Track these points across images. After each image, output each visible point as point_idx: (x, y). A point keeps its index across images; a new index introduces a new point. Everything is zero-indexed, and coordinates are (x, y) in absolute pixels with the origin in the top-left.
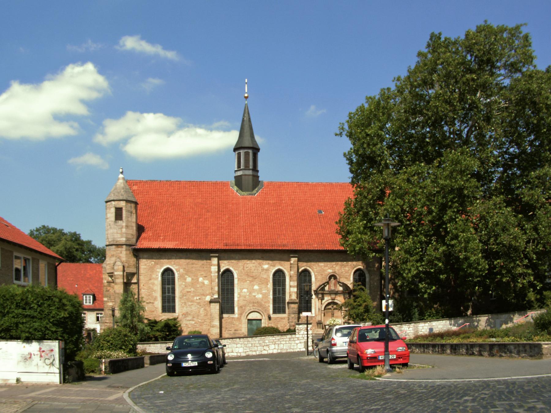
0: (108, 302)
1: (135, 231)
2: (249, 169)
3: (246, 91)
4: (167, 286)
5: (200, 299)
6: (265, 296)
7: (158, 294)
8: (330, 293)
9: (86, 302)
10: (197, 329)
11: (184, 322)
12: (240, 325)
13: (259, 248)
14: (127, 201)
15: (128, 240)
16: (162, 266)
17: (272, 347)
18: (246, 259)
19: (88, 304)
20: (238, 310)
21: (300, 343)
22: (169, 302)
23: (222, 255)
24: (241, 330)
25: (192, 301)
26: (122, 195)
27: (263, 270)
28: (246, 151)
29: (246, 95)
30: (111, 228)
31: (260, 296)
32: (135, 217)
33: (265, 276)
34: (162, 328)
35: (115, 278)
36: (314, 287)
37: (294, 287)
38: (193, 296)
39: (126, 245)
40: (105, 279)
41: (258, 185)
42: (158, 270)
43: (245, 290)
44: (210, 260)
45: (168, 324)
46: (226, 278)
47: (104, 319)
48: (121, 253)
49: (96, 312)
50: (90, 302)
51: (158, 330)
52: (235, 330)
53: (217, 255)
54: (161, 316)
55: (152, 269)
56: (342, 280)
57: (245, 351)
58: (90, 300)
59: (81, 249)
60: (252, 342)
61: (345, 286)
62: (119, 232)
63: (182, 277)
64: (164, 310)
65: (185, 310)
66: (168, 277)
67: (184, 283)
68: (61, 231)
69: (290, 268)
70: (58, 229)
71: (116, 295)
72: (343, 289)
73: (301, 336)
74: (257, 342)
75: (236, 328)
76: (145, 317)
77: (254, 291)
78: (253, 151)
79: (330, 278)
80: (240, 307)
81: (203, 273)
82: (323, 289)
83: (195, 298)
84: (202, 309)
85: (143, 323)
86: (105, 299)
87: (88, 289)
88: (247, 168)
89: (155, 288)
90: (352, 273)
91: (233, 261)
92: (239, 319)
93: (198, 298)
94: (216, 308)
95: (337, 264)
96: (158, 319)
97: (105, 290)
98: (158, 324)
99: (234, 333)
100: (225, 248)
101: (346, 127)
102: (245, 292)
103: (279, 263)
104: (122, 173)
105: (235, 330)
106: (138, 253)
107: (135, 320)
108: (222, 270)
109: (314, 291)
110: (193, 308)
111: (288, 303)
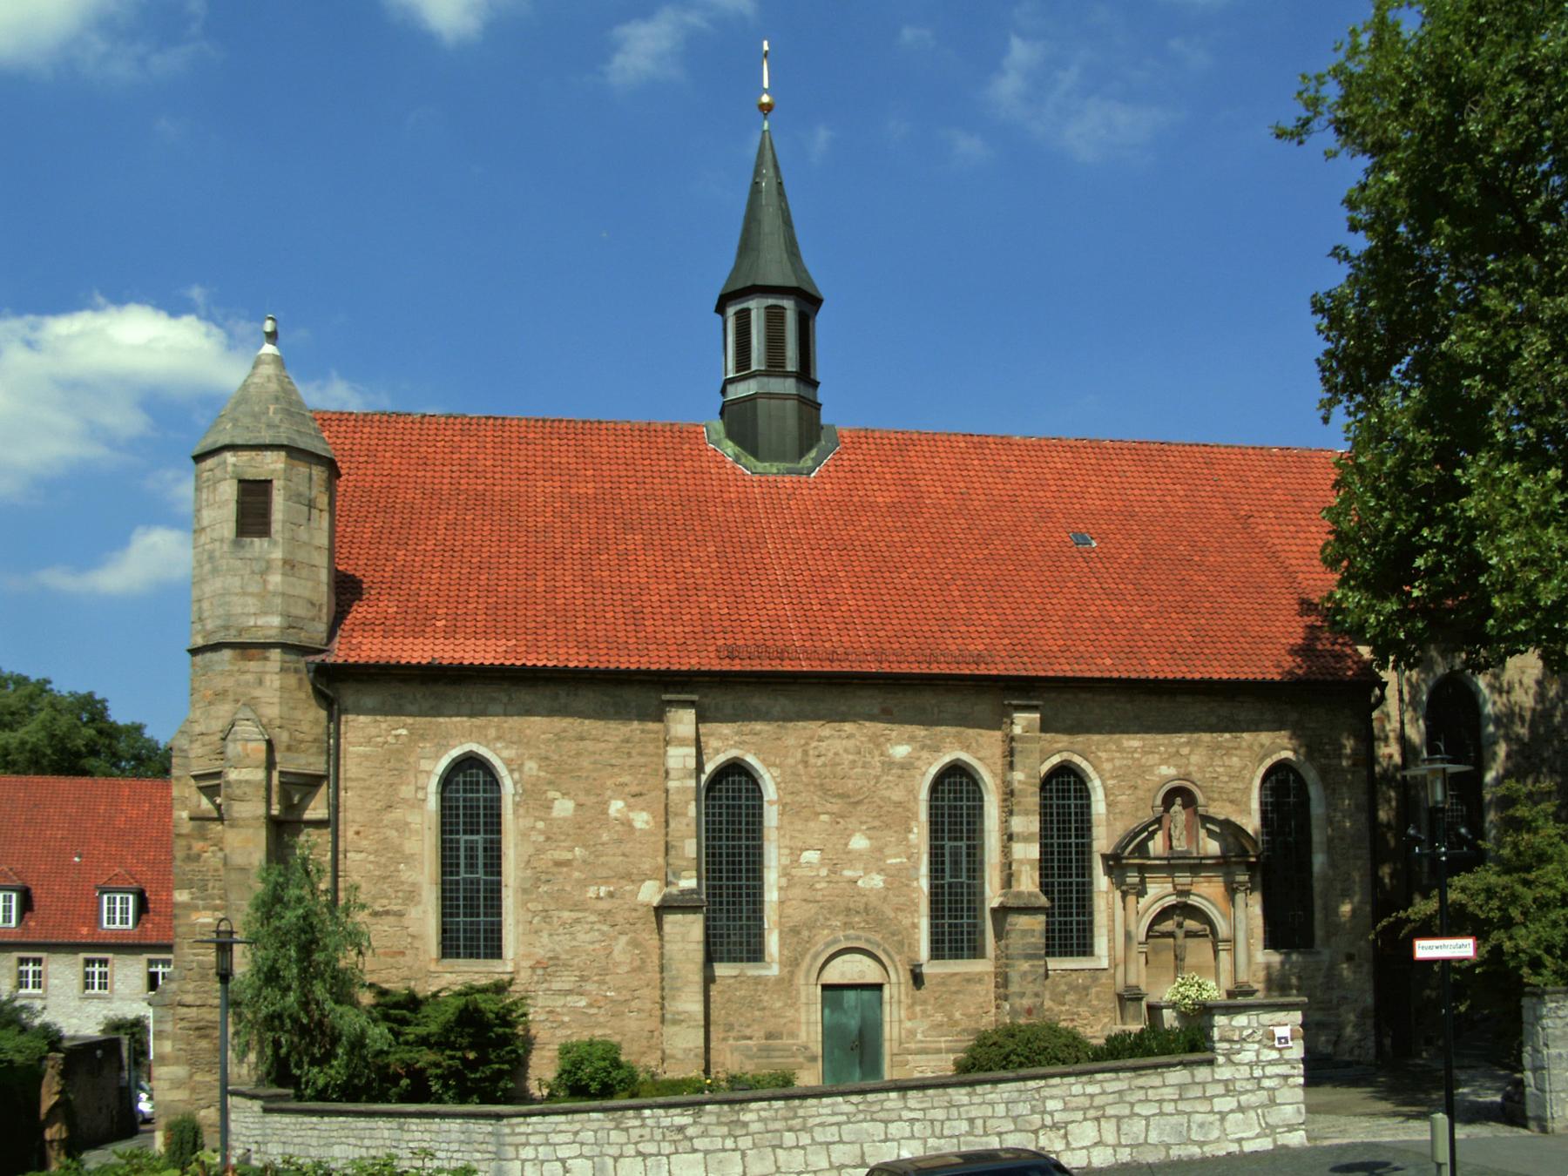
0: (196, 908)
1: (324, 588)
2: (787, 375)
3: (766, 85)
4: (463, 838)
5: (611, 895)
6: (899, 880)
7: (425, 874)
8: (1174, 865)
9: (112, 920)
10: (598, 1032)
11: (540, 1002)
12: (790, 1013)
13: (874, 668)
14: (294, 452)
15: (292, 624)
17: (1085, 1133)
18: (815, 717)
19: (118, 925)
20: (782, 945)
21: (1241, 1109)
22: (472, 910)
23: (713, 699)
24: (793, 1035)
26: (270, 426)
27: (889, 764)
28: (771, 301)
29: (765, 99)
30: (215, 571)
32: (325, 524)
33: (897, 795)
34: (447, 1029)
35: (230, 798)
36: (1102, 841)
37: (1026, 839)
38: (583, 884)
39: (285, 647)
40: (184, 802)
41: (818, 439)
42: (425, 765)
43: (811, 856)
44: (659, 718)
45: (477, 1010)
46: (731, 797)
47: (174, 986)
48: (261, 682)
49: (82, 956)
50: (124, 921)
51: (424, 1041)
52: (769, 1036)
53: (695, 697)
54: (438, 974)
55: (397, 762)
56: (1220, 811)
58: (124, 911)
59: (109, 746)
60: (974, 1112)
61: (1229, 831)
62: (253, 588)
63: (533, 797)
64: (450, 946)
65: (544, 946)
66: (470, 798)
67: (540, 825)
68: (42, 686)
69: (1008, 759)
70: (33, 679)
71: (234, 876)
72: (1225, 849)
73: (1244, 1071)
74: (1001, 1110)
75: (771, 1024)
76: (368, 979)
77: (851, 857)
78: (797, 304)
79: (1168, 800)
80: (791, 932)
81: (626, 779)
82: (1142, 849)
83: (591, 892)
84: (623, 939)
85: (355, 1004)
86: (181, 896)
87: (117, 870)
88: (775, 366)
89: (411, 846)
90: (1257, 782)
91: (758, 726)
92: (785, 984)
93: (603, 891)
94: (688, 932)
95: (1197, 743)
96: (424, 989)
97: (179, 854)
98: (426, 1010)
99: (766, 1051)
100: (726, 666)
101: (1332, 91)
102: (809, 864)
103: (957, 736)
104: (272, 337)
105: (769, 1036)
106: (336, 685)
107: (319, 990)
108: (709, 768)
109: (1105, 857)
110: (581, 937)
111: (1002, 912)
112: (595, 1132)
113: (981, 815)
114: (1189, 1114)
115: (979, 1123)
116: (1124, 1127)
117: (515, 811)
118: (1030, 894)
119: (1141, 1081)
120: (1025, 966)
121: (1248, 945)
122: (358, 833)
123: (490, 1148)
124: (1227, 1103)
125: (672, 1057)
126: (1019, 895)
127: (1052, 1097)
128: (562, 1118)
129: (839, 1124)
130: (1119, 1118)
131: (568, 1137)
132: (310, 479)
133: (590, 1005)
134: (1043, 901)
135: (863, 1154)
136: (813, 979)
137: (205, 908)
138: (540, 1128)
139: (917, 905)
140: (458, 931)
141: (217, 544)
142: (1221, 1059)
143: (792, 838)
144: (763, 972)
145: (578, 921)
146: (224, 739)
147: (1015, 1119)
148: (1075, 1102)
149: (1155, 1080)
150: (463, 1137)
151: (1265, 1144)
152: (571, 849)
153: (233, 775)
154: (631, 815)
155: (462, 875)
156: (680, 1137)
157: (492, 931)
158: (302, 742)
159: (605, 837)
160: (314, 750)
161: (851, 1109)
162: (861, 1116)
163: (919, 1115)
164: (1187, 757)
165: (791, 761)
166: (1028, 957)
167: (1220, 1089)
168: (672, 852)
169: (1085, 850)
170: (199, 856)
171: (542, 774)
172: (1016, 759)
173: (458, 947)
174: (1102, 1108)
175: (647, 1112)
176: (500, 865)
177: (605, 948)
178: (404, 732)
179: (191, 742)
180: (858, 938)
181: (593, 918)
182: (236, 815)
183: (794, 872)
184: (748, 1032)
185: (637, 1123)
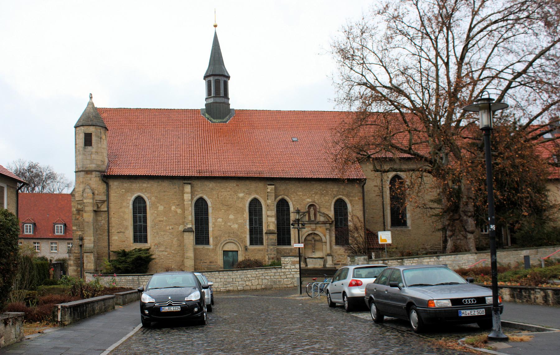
0: (78, 231)
4: (138, 215)
5: (172, 228)
6: (241, 226)
12: (215, 257)
16: (133, 194)
20: (213, 241)
24: (216, 262)
25: (164, 231)
27: (239, 198)
31: (236, 226)
33: (241, 205)
37: (271, 217)
42: (129, 198)
46: (201, 208)
50: (61, 232)
52: (211, 262)
64: (136, 240)
66: (139, 206)
67: (156, 212)
74: (238, 276)
80: (215, 238)
81: (176, 201)
83: (168, 228)
86: (74, 228)
90: (333, 203)
92: (214, 250)
93: (170, 227)
94: (190, 238)
102: (220, 222)
113: (262, 210)
119: (267, 272)
120: (272, 247)
121: (330, 244)
148: (253, 276)
153: (85, 201)
166: (272, 245)
167: (283, 274)
181: (168, 234)
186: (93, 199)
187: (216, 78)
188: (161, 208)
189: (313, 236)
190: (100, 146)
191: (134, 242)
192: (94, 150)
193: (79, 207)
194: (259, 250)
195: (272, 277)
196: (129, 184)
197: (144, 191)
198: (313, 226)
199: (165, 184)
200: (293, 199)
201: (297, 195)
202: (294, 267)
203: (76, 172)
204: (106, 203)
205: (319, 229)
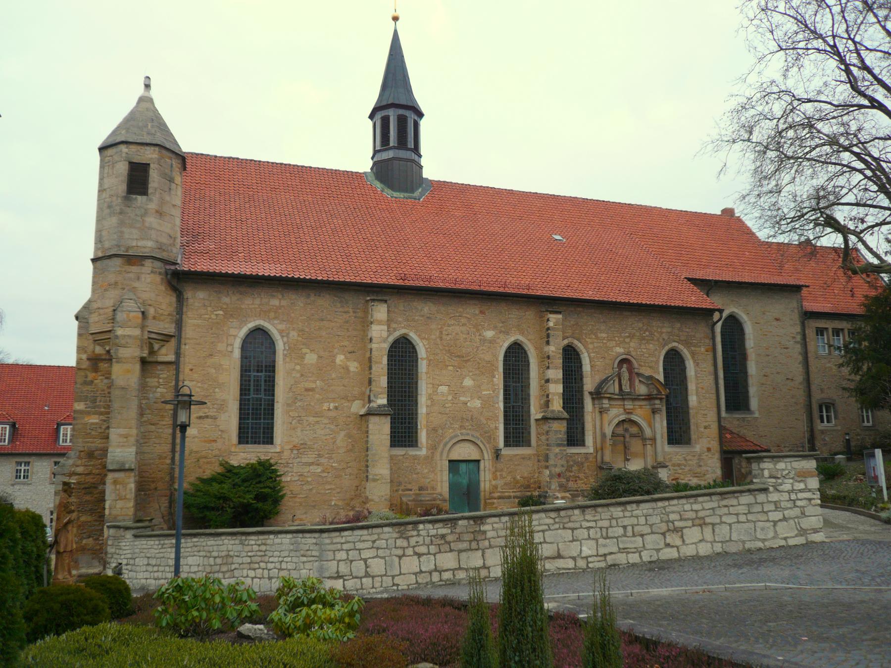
2: (391, 148)
5: (336, 408)
8: (623, 396)
12: (432, 476)
16: (243, 323)
17: (693, 534)
21: (785, 519)
24: (433, 488)
25: (316, 415)
27: (483, 340)
33: (488, 357)
36: (589, 385)
37: (556, 382)
42: (233, 332)
43: (443, 389)
46: (402, 355)
48: (138, 279)
52: (421, 489)
56: (647, 372)
57: (602, 551)
60: (626, 522)
61: (650, 380)
64: (244, 437)
67: (298, 367)
73: (786, 496)
74: (642, 520)
81: (346, 343)
90: (662, 358)
92: (429, 459)
93: (332, 406)
94: (380, 429)
100: (401, 283)
102: (443, 394)
105: (421, 489)
109: (591, 393)
112: (387, 540)
114: (754, 522)
115: (629, 529)
116: (717, 530)
117: (284, 359)
118: (559, 411)
119: (724, 502)
122: (191, 370)
123: (314, 553)
124: (776, 516)
125: (372, 500)
126: (553, 411)
127: (673, 512)
128: (365, 532)
129: (543, 531)
130: (713, 525)
131: (369, 544)
132: (172, 166)
133: (323, 471)
134: (566, 415)
135: (559, 550)
136: (444, 457)
137: (94, 414)
138: (350, 539)
139: (498, 417)
140: (248, 428)
141: (115, 198)
142: (771, 489)
143: (434, 378)
144: (418, 453)
145: (317, 422)
146: (114, 310)
147: (651, 526)
149: (734, 502)
150: (292, 547)
151: (801, 540)
152: (315, 382)
154: (348, 363)
155: (252, 396)
156: (443, 542)
157: (268, 428)
158: (162, 315)
159: (334, 376)
160: (168, 320)
161: (551, 521)
162: (557, 526)
163: (592, 524)
164: (629, 343)
165: (433, 337)
166: (559, 445)
167: (772, 507)
168: (373, 384)
169: (580, 390)
170: (92, 382)
171: (300, 339)
172: (551, 339)
173: (248, 437)
174: (703, 518)
175: (421, 526)
176: (273, 390)
177: (332, 438)
178: (221, 312)
179: (91, 313)
180: (468, 434)
181: (326, 421)
182: (120, 355)
183: (434, 398)
184: (409, 486)
185: (415, 533)
186: (143, 327)
187: (401, 112)
188: (311, 358)
189: (626, 426)
190: (167, 198)
191: (240, 442)
192: (152, 206)
193: (99, 350)
194: (523, 458)
195: (742, 518)
196: (234, 298)
197: (272, 315)
198: (629, 405)
199: (324, 302)
200: (591, 346)
201: (597, 338)
202: (802, 486)
203: (94, 260)
204: (173, 342)
205: (639, 411)
